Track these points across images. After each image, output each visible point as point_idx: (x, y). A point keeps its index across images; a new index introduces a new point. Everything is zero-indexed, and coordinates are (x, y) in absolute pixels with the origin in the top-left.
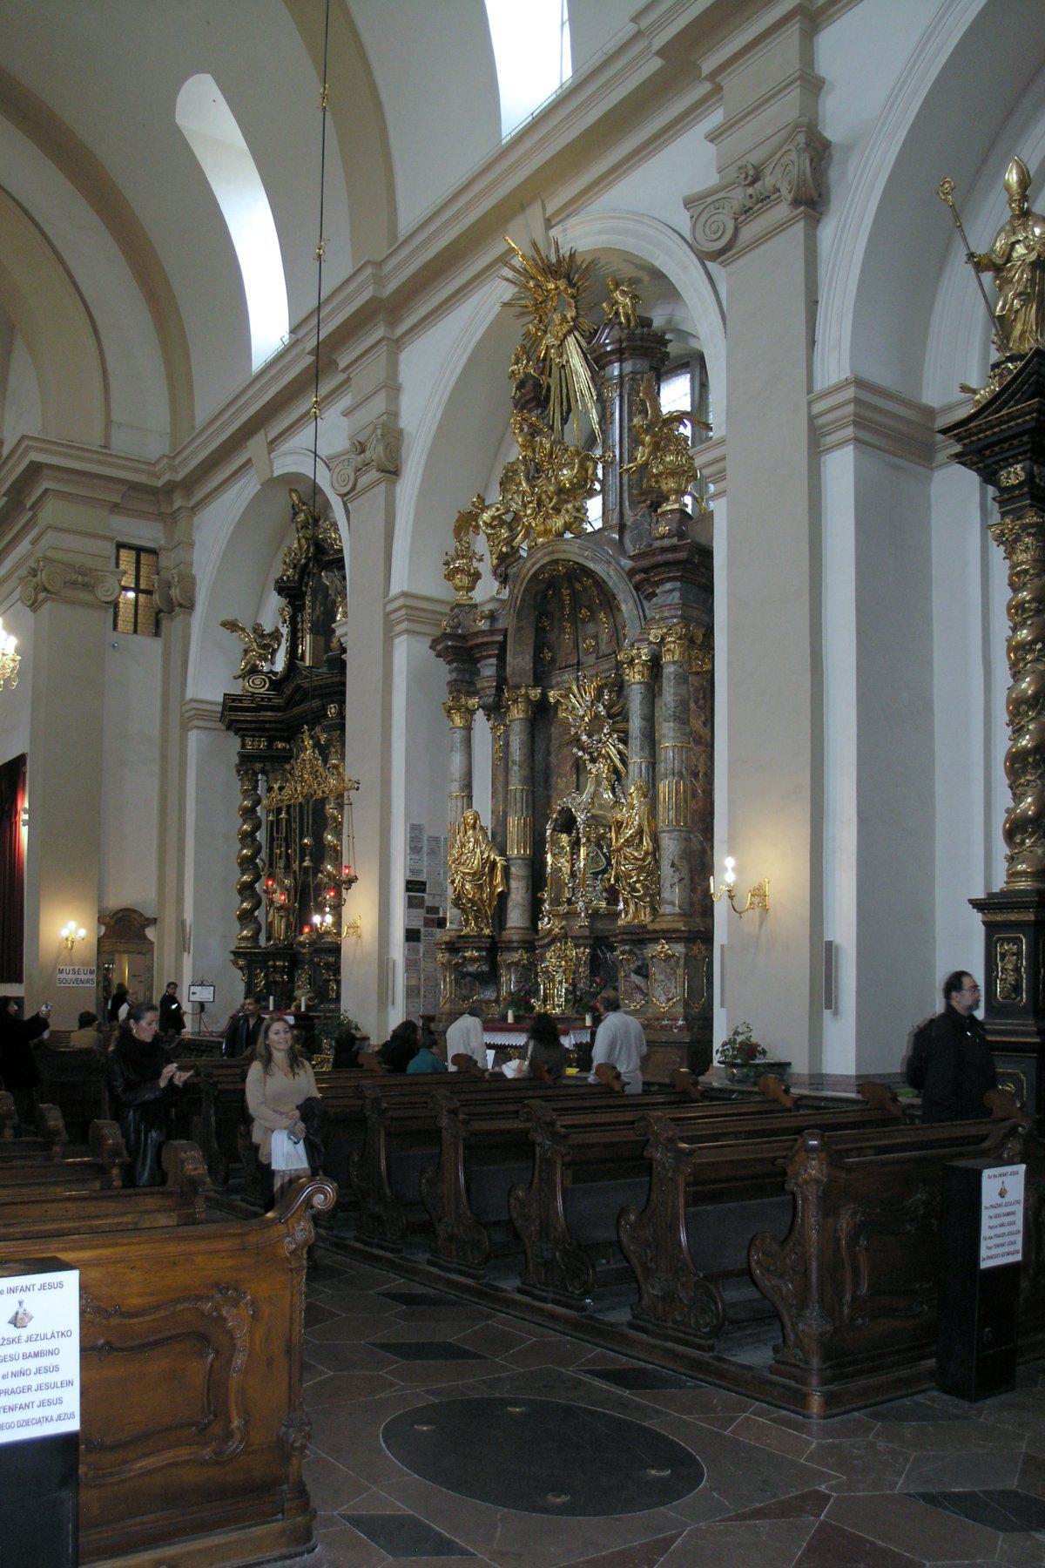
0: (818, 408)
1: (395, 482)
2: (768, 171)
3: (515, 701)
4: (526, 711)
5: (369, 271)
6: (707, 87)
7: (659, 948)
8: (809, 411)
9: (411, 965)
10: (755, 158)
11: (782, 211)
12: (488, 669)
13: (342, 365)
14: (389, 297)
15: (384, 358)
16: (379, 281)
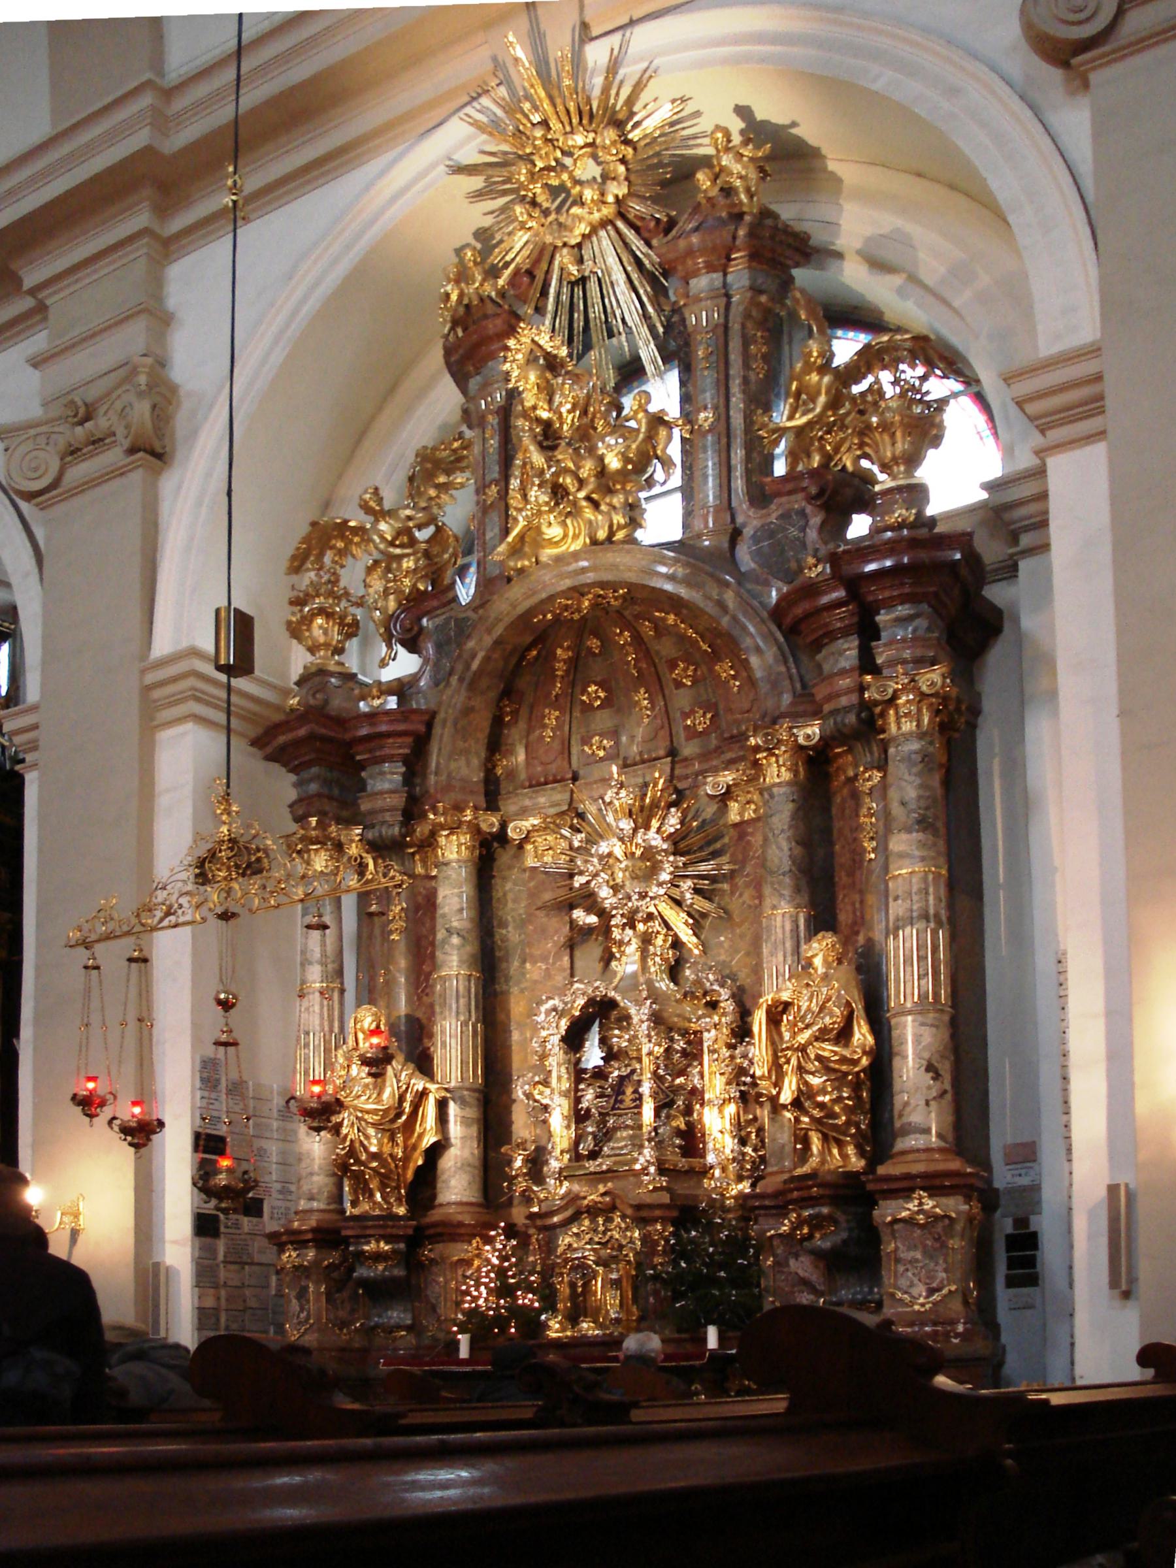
0: (150, 678)
1: (158, 473)
2: (102, 411)
3: (453, 829)
4: (472, 849)
5: (146, 100)
6: (29, 303)
7: (913, 1206)
8: (141, 680)
9: (204, 1274)
10: (92, 394)
11: (114, 456)
12: (386, 781)
13: (28, 283)
14: (176, 156)
15: (141, 266)
16: (161, 121)
